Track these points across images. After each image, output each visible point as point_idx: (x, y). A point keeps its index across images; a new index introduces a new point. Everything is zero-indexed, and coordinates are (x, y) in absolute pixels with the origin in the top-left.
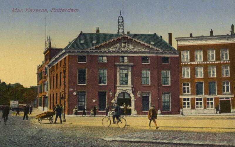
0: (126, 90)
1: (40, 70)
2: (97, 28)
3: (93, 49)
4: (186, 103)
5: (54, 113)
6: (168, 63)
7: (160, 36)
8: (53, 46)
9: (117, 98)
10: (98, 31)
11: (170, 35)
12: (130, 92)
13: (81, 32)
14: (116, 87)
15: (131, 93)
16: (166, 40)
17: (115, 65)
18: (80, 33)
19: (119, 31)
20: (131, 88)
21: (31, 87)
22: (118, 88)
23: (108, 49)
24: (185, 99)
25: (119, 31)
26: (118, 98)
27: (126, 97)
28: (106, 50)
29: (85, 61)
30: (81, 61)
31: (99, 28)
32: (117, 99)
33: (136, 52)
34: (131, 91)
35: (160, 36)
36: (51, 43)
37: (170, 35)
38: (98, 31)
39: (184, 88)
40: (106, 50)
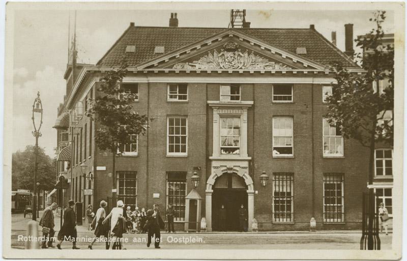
0: (235, 168)
1: (63, 114)
2: (172, 14)
3: (152, 66)
4: (384, 202)
5: (140, 207)
6: (274, 100)
7: (166, 23)
8: (78, 61)
9: (213, 187)
10: (174, 21)
11: (349, 29)
12: (244, 173)
13: (132, 24)
14: (211, 160)
15: (247, 175)
16: (341, 45)
17: (208, 105)
18: (128, 25)
19: (232, 22)
20: (246, 164)
21: (48, 156)
22: (214, 164)
23: (192, 66)
24: (380, 191)
25: (232, 22)
26: (216, 187)
27: (235, 186)
28: (188, 68)
29: (290, 98)
30: (280, 98)
31: (176, 14)
32: (212, 191)
33: (258, 74)
34: (247, 170)
35: (166, 23)
36: (77, 52)
37: (349, 29)
38: (174, 21)
39: (380, 164)
40: (188, 68)
